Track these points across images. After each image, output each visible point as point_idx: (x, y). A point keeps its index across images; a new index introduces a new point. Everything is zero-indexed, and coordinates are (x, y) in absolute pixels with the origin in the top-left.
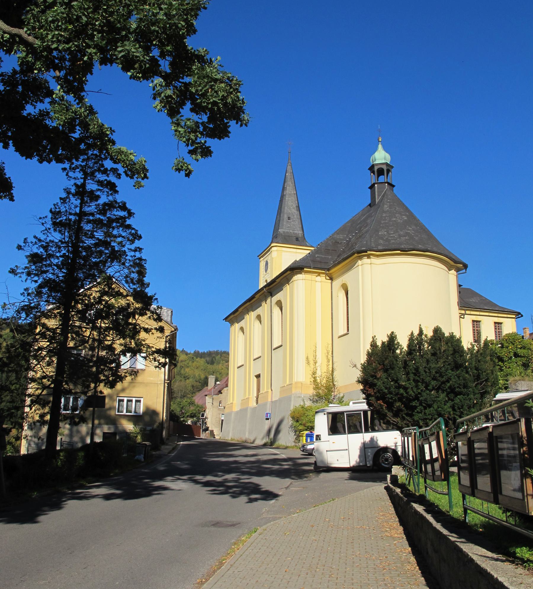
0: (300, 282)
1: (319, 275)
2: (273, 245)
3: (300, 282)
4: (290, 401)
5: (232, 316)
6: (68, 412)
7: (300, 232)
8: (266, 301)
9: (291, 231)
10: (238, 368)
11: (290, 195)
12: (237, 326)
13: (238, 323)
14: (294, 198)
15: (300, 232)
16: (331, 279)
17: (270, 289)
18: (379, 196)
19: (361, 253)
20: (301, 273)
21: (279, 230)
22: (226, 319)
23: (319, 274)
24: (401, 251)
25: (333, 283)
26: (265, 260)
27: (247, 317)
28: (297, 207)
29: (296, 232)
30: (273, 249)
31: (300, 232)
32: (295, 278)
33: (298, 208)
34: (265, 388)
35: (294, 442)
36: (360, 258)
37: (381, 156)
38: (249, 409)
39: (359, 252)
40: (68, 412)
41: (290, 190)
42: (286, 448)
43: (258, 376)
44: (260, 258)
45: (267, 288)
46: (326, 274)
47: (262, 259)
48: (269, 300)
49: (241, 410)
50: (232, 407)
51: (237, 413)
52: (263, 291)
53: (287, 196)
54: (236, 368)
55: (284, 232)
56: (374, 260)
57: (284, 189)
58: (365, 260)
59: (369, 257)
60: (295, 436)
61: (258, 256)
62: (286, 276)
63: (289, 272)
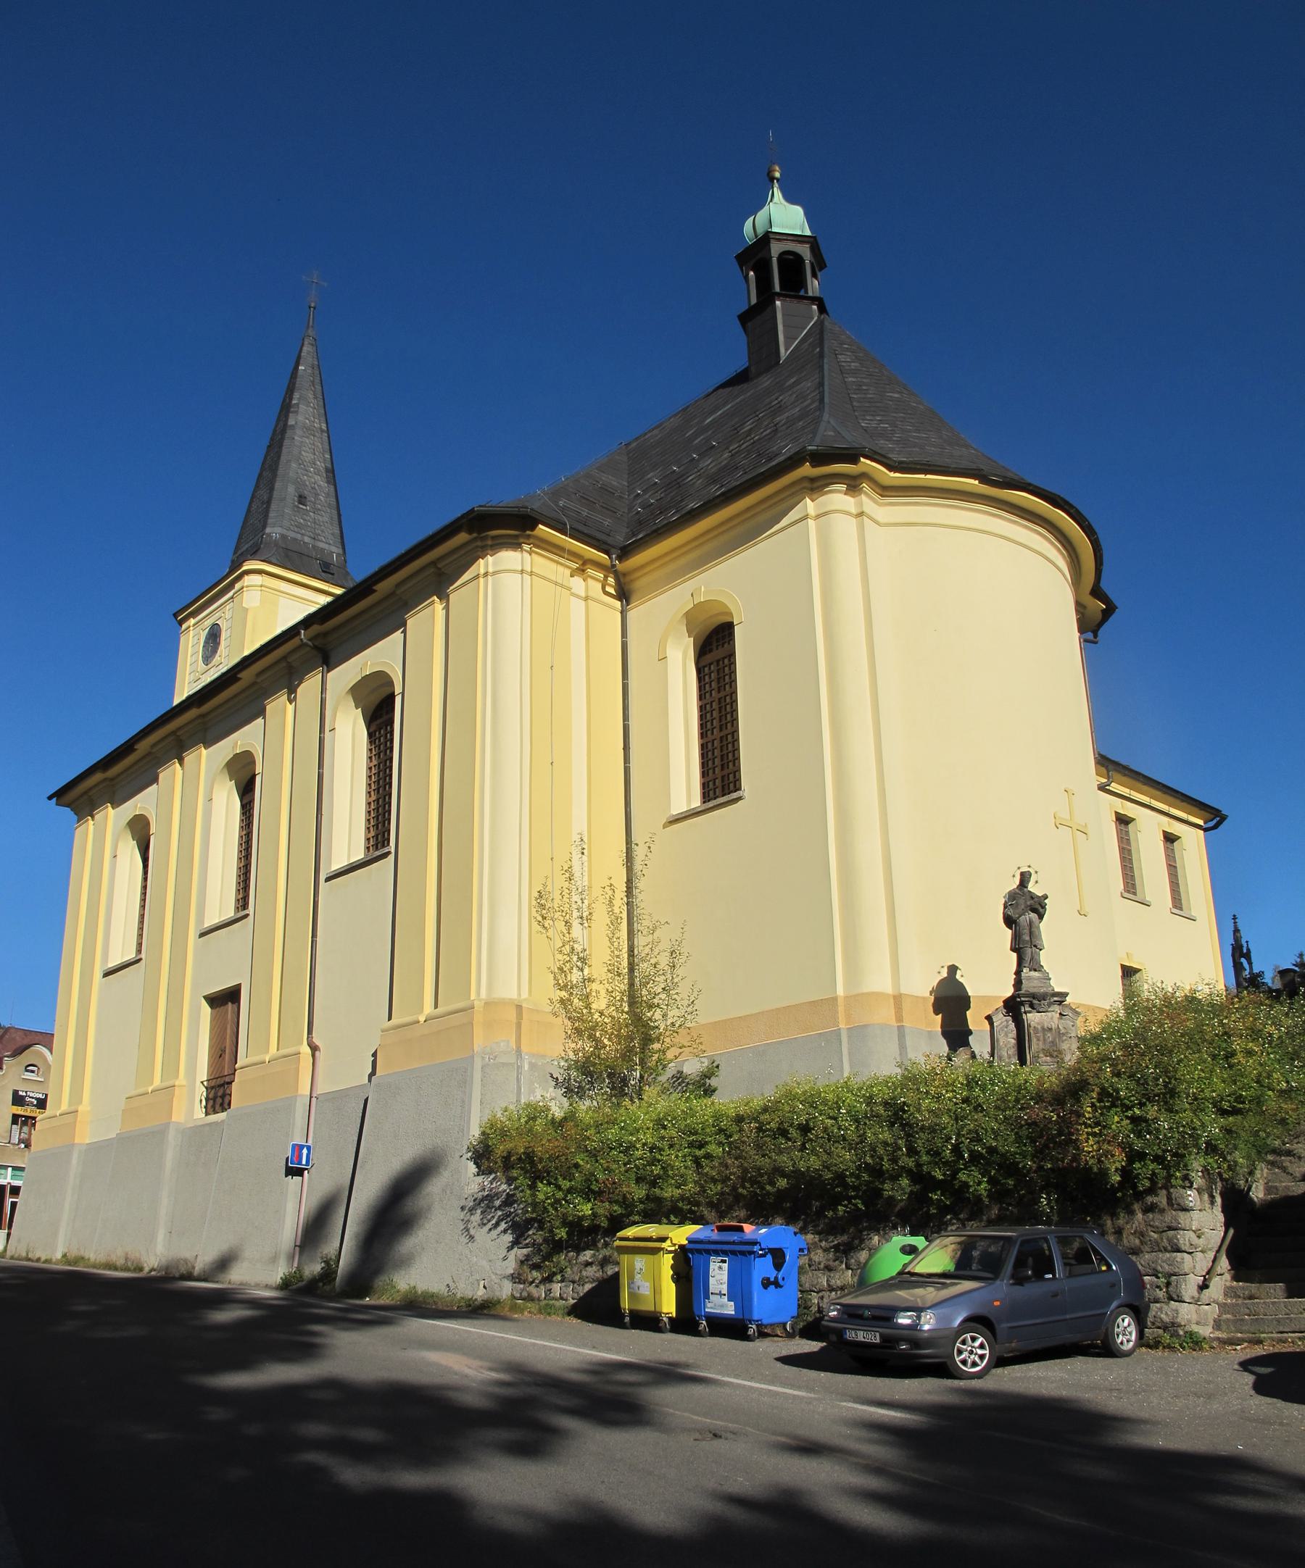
0: (511, 581)
1: (581, 571)
2: (247, 566)
3: (511, 581)
4: (465, 1083)
5: (98, 776)
6: (161, 1236)
7: (334, 549)
8: (292, 691)
9: (307, 539)
10: (107, 974)
11: (309, 430)
12: (112, 818)
13: (115, 804)
14: (319, 443)
15: (336, 550)
16: (624, 595)
17: (325, 634)
18: (789, 340)
19: (830, 460)
20: (516, 545)
21: (268, 530)
22: (59, 795)
23: (583, 566)
24: (984, 479)
25: (632, 615)
26: (209, 622)
27: (173, 774)
28: (327, 470)
29: (321, 545)
30: (248, 580)
31: (334, 549)
32: (487, 563)
33: (331, 474)
34: (263, 1039)
35: (516, 1278)
36: (816, 486)
37: (784, 216)
38: (172, 1136)
39: (820, 458)
40: (161, 1236)
41: (306, 414)
42: (479, 1310)
43: (226, 1000)
44: (181, 623)
45: (316, 628)
46: (609, 570)
47: (192, 621)
48: (309, 687)
49: (122, 1140)
50: (73, 1126)
51: (97, 1149)
52: (294, 643)
53: (299, 432)
54: (98, 974)
55: (283, 537)
56: (868, 501)
57: (286, 408)
58: (837, 498)
59: (853, 484)
60: (521, 1252)
61: (175, 615)
62: (433, 563)
63: (463, 537)
